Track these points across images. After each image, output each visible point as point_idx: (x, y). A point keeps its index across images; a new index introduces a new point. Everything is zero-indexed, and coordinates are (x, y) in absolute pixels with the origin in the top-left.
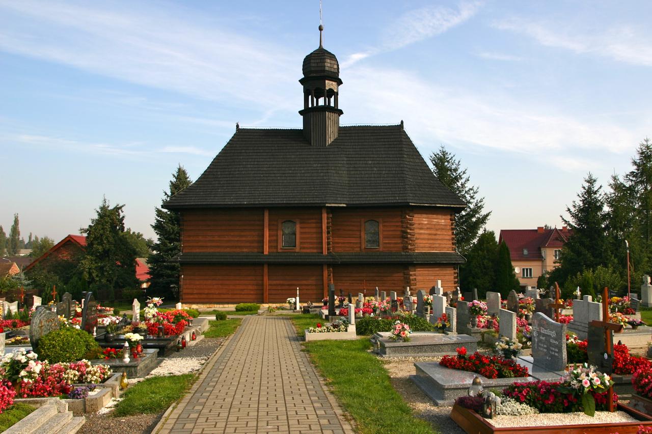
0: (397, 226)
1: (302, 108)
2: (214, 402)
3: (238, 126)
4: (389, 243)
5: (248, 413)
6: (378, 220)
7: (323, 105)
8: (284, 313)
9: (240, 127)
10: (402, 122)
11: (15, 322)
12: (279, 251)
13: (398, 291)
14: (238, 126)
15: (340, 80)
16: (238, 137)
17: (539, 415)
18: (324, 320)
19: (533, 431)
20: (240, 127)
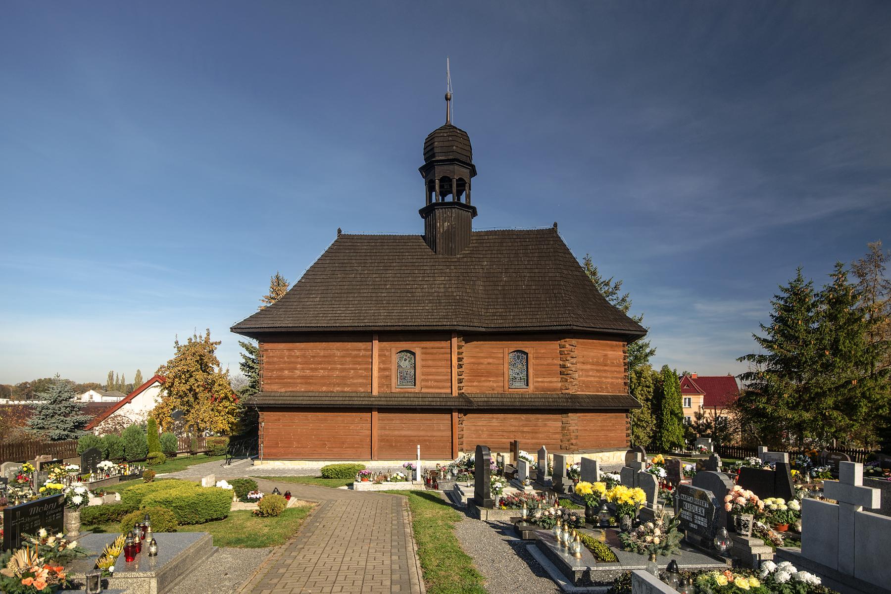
0: (617, 378)
1: (424, 205)
2: (305, 555)
3: (339, 231)
4: (542, 382)
5: (354, 581)
6: (526, 351)
7: (452, 201)
8: (345, 403)
9: (343, 233)
10: (555, 225)
11: (5, 553)
12: (393, 391)
13: (735, 542)
14: (339, 231)
15: (473, 167)
16: (339, 244)
17: (720, 576)
18: (419, 442)
19: (323, 323)
20: (343, 233)
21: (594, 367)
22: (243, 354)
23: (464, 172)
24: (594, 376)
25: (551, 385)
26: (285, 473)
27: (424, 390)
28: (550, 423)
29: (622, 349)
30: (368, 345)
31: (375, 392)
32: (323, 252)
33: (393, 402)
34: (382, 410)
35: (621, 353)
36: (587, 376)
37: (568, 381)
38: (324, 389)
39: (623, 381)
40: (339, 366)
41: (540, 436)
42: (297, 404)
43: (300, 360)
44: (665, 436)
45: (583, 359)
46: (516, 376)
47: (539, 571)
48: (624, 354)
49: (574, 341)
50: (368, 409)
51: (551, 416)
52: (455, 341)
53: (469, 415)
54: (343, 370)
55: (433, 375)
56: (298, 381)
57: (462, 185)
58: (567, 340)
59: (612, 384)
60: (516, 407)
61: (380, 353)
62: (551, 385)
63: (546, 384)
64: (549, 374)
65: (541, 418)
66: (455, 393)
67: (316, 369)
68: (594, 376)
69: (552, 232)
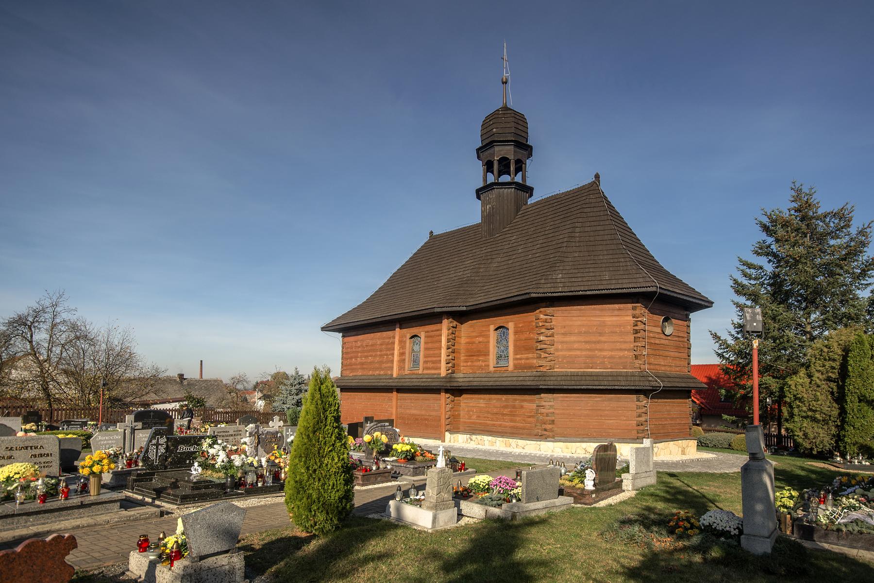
14: (431, 232)
21: (581, 339)
22: (713, 332)
23: (521, 154)
24: (581, 350)
25: (528, 361)
26: (688, 467)
27: (426, 372)
28: (525, 404)
29: (631, 312)
30: (390, 333)
31: (395, 376)
32: (411, 255)
33: (407, 383)
34: (400, 390)
35: (630, 318)
36: (570, 350)
37: (542, 356)
38: (371, 373)
39: (632, 354)
40: (379, 353)
41: (518, 419)
42: (678, 387)
43: (360, 349)
44: (849, 435)
45: (565, 330)
46: (501, 354)
47: (90, 507)
48: (635, 319)
49: (550, 310)
50: (388, 390)
51: (527, 397)
52: (445, 322)
53: (464, 396)
54: (381, 356)
55: (431, 357)
56: (359, 367)
57: (520, 166)
58: (542, 309)
59: (611, 357)
60: (550, 387)
61: (488, 333)
62: (528, 361)
63: (523, 361)
64: (527, 349)
65: (518, 399)
66: (443, 372)
67: (366, 357)
68: (581, 350)
69: (593, 189)
